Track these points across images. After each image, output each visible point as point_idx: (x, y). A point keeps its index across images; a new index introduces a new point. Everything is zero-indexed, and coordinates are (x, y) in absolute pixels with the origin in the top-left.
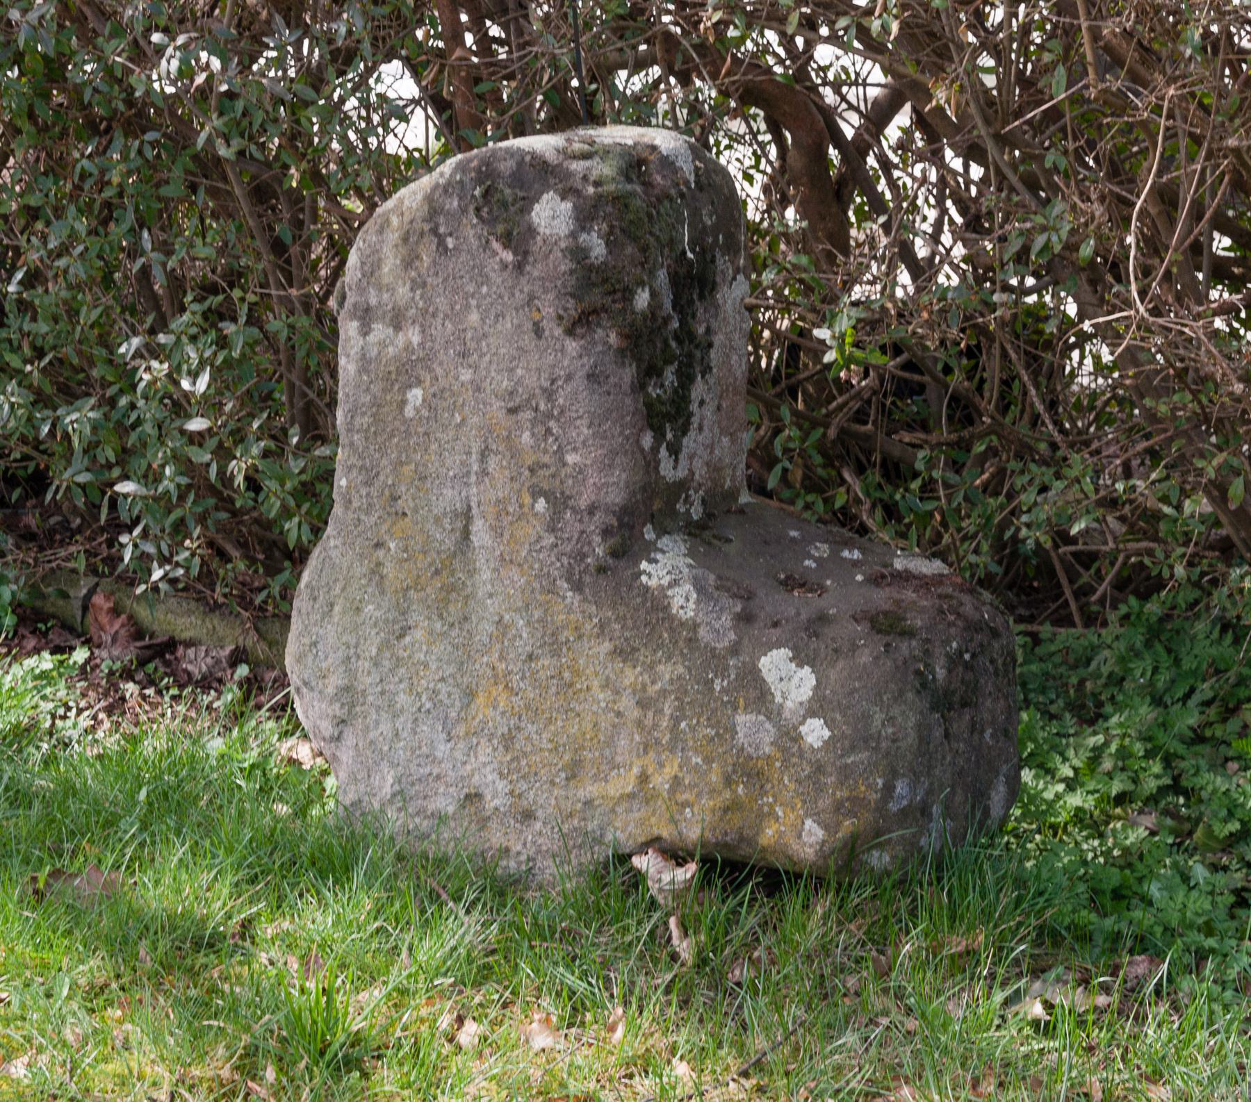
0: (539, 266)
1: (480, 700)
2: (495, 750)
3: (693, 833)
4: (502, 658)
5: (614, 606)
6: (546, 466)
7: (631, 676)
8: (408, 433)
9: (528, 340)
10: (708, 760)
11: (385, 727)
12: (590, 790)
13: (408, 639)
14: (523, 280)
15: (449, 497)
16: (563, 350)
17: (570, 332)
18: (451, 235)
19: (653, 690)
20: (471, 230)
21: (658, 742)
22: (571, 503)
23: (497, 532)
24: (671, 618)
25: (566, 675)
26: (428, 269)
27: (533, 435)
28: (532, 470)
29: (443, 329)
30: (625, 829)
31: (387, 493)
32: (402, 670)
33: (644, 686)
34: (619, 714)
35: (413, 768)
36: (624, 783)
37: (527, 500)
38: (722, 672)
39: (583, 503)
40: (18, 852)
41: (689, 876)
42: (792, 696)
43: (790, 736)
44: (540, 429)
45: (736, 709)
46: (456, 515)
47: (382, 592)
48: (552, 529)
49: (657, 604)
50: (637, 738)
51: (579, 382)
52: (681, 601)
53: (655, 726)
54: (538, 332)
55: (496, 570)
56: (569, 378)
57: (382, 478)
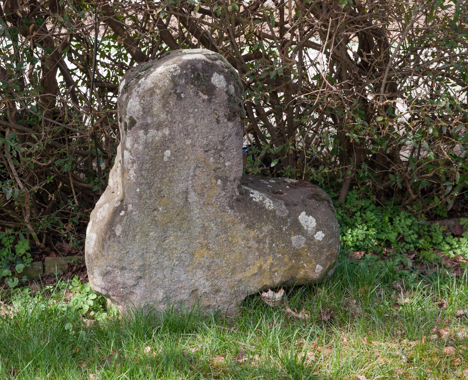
0: (218, 99)
1: (197, 255)
2: (204, 272)
3: (277, 280)
4: (205, 239)
5: (245, 212)
6: (220, 168)
7: (252, 233)
8: (166, 167)
9: (214, 125)
10: (283, 255)
11: (160, 275)
12: (239, 276)
13: (167, 241)
14: (212, 105)
15: (181, 186)
16: (227, 127)
17: (229, 120)
18: (182, 93)
19: (261, 236)
20: (191, 90)
21: (265, 253)
22: (229, 179)
23: (201, 195)
24: (266, 210)
25: (230, 239)
26: (173, 106)
27: (214, 158)
28: (215, 171)
29: (178, 127)
30: (253, 287)
31: (157, 190)
32: (166, 253)
33: (258, 236)
34: (249, 247)
35: (172, 287)
36: (255, 270)
37: (214, 181)
38: (285, 223)
39: (232, 179)
40: (21, 361)
41: (282, 294)
42: (310, 226)
43: (311, 239)
44: (217, 156)
45: (290, 235)
46: (183, 192)
47: (157, 227)
48: (224, 189)
49: (260, 207)
50: (257, 254)
51: (233, 136)
52: (269, 204)
53: (264, 248)
54: (218, 122)
55: (201, 208)
56: (230, 136)
57: (155, 185)
